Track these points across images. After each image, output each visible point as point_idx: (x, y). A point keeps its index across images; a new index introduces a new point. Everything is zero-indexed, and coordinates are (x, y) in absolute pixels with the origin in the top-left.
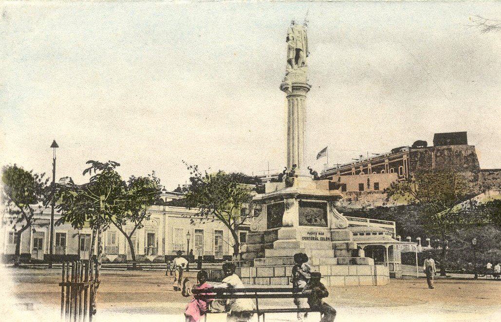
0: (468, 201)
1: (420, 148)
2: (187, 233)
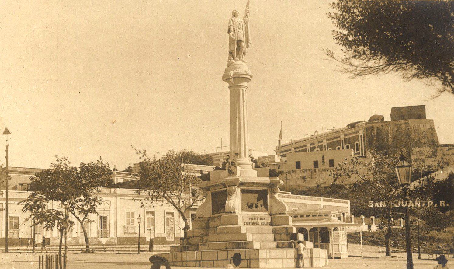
0: (425, 177)
1: (376, 123)
2: (138, 217)
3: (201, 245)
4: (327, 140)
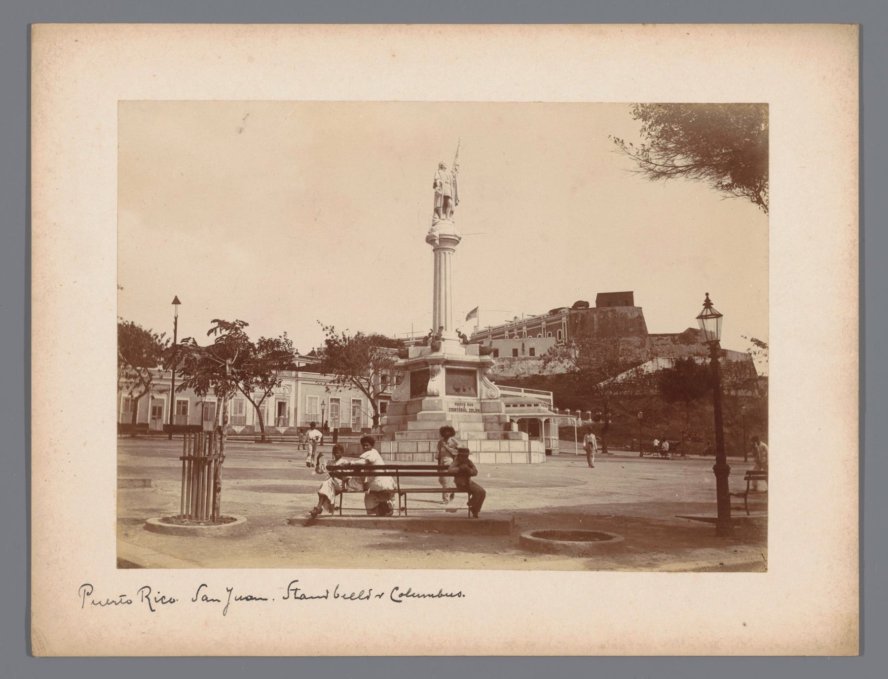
3: (398, 434)
4: (527, 327)
